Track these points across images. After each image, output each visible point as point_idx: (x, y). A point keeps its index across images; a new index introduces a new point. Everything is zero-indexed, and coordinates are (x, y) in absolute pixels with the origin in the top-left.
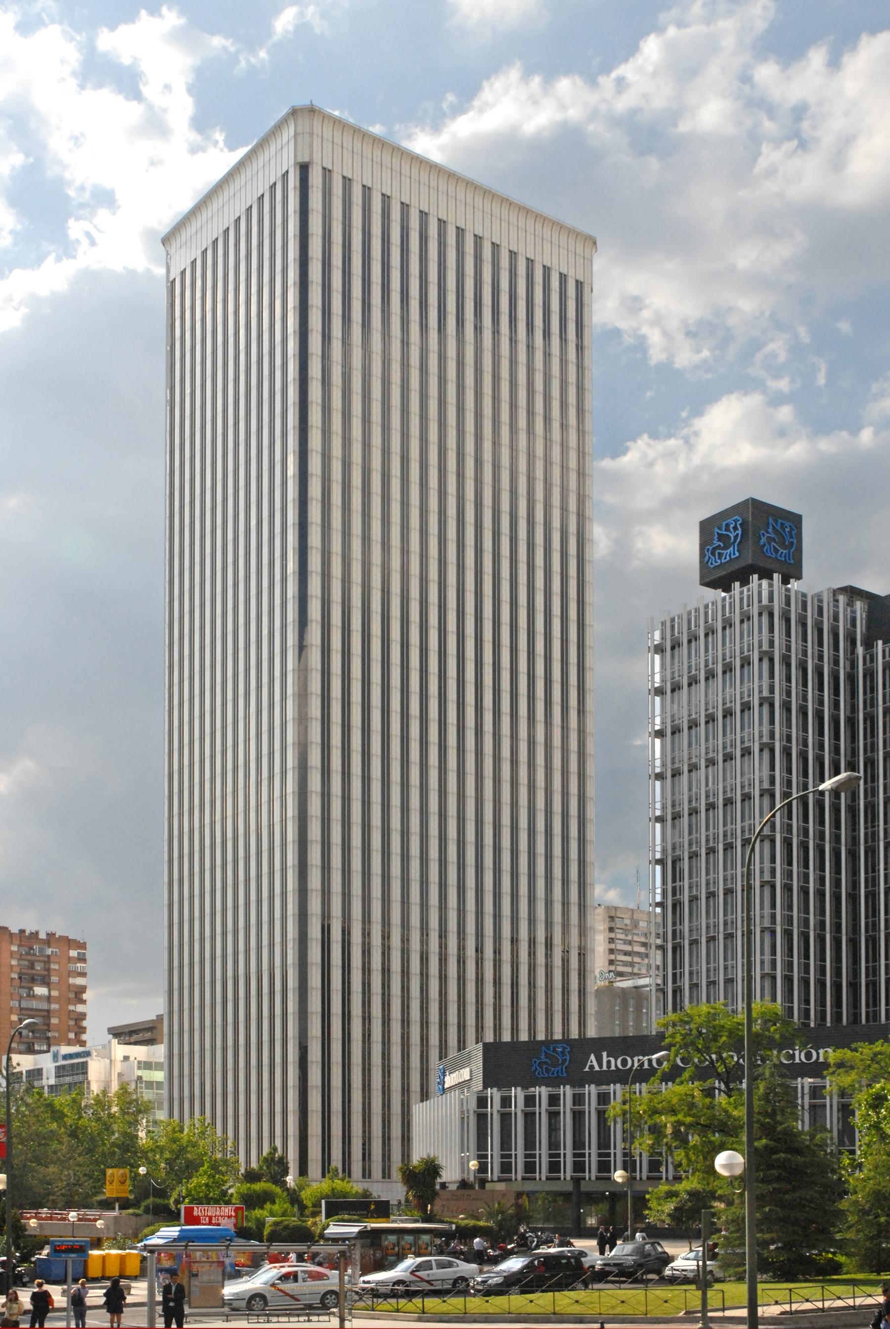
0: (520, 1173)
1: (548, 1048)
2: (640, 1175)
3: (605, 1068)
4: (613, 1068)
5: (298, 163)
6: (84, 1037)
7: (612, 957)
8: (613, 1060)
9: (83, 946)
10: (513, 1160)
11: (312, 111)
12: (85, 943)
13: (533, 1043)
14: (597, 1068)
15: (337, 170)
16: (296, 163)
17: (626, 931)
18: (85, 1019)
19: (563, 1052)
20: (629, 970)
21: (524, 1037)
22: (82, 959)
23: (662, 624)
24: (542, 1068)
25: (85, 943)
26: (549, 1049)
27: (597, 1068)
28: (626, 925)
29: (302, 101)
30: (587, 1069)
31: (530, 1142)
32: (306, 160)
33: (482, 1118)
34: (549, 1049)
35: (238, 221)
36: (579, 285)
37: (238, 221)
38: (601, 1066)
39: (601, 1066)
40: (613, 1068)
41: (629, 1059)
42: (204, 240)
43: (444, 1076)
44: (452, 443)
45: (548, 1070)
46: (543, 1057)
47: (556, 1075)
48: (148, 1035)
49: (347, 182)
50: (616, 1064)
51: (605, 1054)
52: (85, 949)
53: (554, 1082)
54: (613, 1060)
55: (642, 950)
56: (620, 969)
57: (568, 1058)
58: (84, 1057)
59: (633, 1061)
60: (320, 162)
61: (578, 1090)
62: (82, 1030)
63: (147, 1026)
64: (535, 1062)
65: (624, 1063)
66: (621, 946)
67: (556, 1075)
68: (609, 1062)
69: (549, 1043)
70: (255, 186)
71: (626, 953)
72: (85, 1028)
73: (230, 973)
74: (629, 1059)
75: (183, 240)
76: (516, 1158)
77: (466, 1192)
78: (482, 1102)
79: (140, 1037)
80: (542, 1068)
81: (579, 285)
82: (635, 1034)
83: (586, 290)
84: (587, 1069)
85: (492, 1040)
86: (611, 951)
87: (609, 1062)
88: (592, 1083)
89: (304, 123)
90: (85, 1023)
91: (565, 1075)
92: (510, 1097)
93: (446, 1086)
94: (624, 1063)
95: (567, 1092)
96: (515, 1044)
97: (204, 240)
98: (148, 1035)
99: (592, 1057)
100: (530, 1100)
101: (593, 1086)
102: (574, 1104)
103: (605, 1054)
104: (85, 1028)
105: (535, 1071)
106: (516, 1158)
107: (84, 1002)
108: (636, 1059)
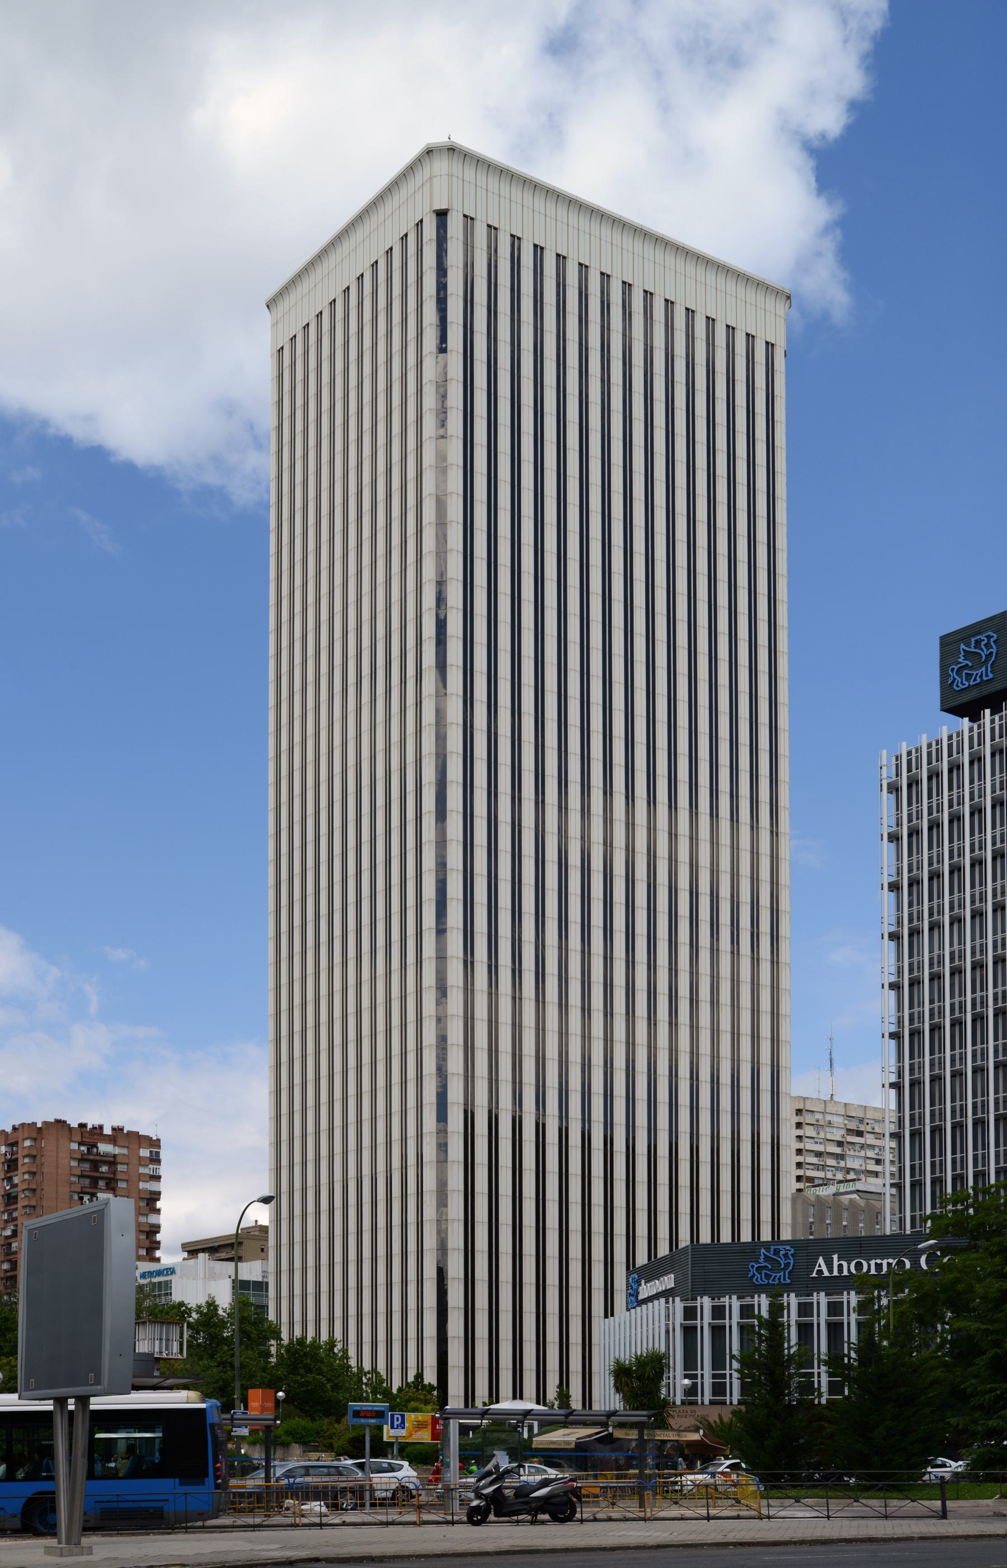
0: (708, 1397)
3: (836, 1273)
4: (845, 1273)
5: (435, 211)
6: (158, 1254)
8: (845, 1264)
9: (155, 1144)
10: (728, 1380)
11: (452, 150)
12: (159, 1140)
14: (826, 1273)
17: (817, 1126)
18: (159, 1232)
19: (786, 1256)
20: (820, 1174)
22: (156, 1159)
23: (897, 758)
24: (760, 1274)
25: (159, 1140)
26: (769, 1252)
27: (826, 1273)
28: (818, 1121)
29: (438, 138)
30: (814, 1275)
32: (444, 207)
34: (769, 1252)
38: (831, 1271)
39: (831, 1271)
40: (845, 1273)
41: (853, 1271)
46: (762, 1260)
47: (777, 1282)
48: (232, 1254)
49: (627, 287)
50: (849, 1268)
51: (835, 1257)
52: (159, 1147)
54: (845, 1264)
55: (838, 1150)
56: (810, 1173)
57: (792, 1262)
58: (167, 1275)
59: (869, 1266)
61: (805, 1299)
62: (155, 1245)
64: (753, 1266)
65: (859, 1266)
66: (810, 1146)
67: (777, 1282)
68: (840, 1266)
71: (819, 1154)
72: (159, 1243)
74: (853, 1271)
77: (689, 1408)
78: (690, 1313)
79: (223, 1255)
80: (760, 1274)
82: (868, 1234)
84: (814, 1275)
86: (799, 1152)
87: (840, 1266)
89: (441, 165)
90: (158, 1237)
91: (788, 1281)
93: (641, 1297)
94: (859, 1266)
98: (232, 1254)
99: (821, 1261)
103: (835, 1257)
104: (159, 1243)
105: (753, 1277)
107: (158, 1211)
108: (873, 1263)
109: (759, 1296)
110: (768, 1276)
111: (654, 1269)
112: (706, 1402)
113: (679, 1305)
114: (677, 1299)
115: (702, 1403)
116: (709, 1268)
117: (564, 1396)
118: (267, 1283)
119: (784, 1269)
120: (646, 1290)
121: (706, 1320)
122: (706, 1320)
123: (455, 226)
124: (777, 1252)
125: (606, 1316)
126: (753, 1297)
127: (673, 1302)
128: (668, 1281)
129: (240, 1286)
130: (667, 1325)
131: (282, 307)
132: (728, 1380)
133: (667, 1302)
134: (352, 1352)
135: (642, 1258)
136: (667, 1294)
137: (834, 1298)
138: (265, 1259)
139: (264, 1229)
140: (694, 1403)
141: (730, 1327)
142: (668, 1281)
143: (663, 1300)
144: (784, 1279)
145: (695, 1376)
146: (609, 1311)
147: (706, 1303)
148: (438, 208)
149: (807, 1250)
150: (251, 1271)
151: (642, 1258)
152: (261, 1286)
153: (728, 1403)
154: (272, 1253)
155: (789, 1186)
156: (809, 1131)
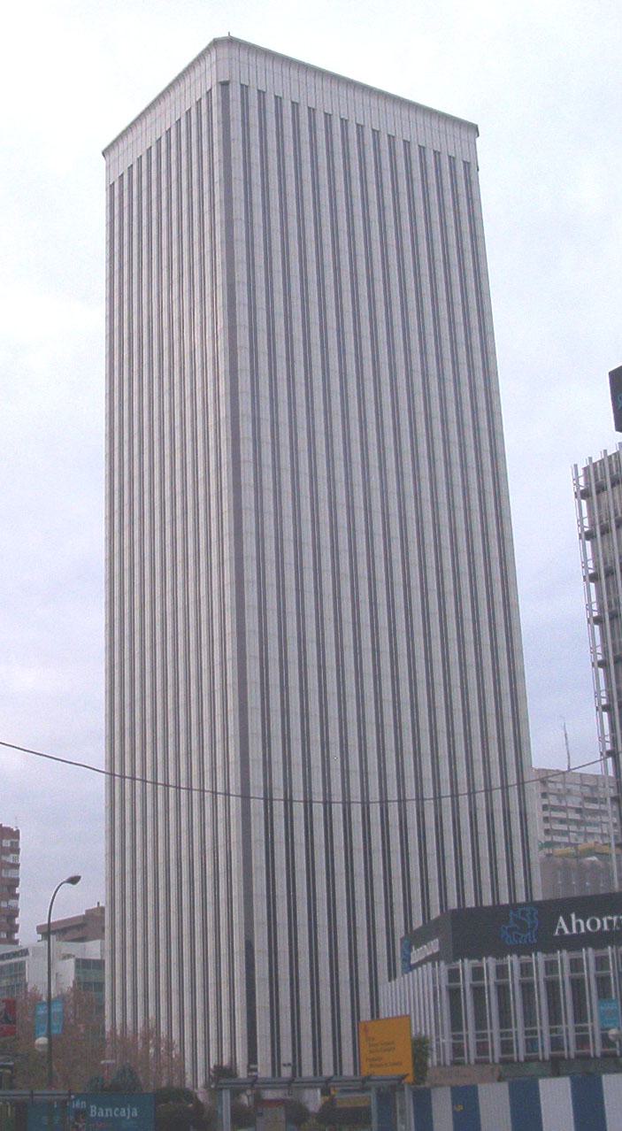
0: (473, 1055)
1: (515, 911)
2: (468, 1058)
7: (547, 814)
10: (539, 1036)
13: (497, 908)
15: (253, 85)
16: (217, 83)
21: (487, 901)
30: (557, 933)
31: (529, 1018)
33: (454, 994)
35: (199, 103)
36: (467, 164)
37: (199, 103)
42: (209, 81)
43: (410, 950)
44: (439, 255)
45: (518, 937)
53: (500, 954)
60: (238, 80)
61: (500, 962)
63: (75, 923)
64: (504, 928)
69: (514, 906)
70: (193, 93)
73: (173, 856)
75: (158, 113)
76: (516, 1035)
78: (454, 975)
81: (467, 164)
83: (473, 168)
85: (456, 907)
88: (538, 951)
91: (535, 941)
92: (531, 963)
95: (539, 959)
96: (479, 909)
97: (198, 92)
100: (501, 971)
101: (515, 957)
102: (547, 973)
106: (516, 1035)
109: (487, 959)
110: (518, 937)
111: (415, 938)
112: (472, 1062)
113: (443, 967)
114: (442, 964)
115: (469, 1063)
116: (473, 931)
117: (296, 1065)
118: (104, 962)
119: (532, 929)
120: (417, 955)
121: (467, 982)
122: (467, 982)
123: (235, 93)
124: (523, 913)
125: (390, 980)
126: (480, 959)
127: (439, 965)
128: (433, 946)
129: (83, 964)
130: (435, 988)
131: (114, 154)
132: (539, 1036)
133: (434, 966)
134: (163, 1028)
135: (418, 922)
136: (433, 958)
137: (551, 957)
138: (103, 938)
139: (102, 910)
140: (487, 1062)
141: (489, 987)
142: (433, 946)
143: (430, 964)
144: (532, 939)
145: (461, 1037)
146: (392, 975)
147: (466, 965)
148: (222, 80)
149: (551, 910)
150: (93, 949)
151: (418, 922)
152: (99, 964)
153: (491, 1061)
154: (107, 932)
155: (536, 856)
156: (553, 801)
